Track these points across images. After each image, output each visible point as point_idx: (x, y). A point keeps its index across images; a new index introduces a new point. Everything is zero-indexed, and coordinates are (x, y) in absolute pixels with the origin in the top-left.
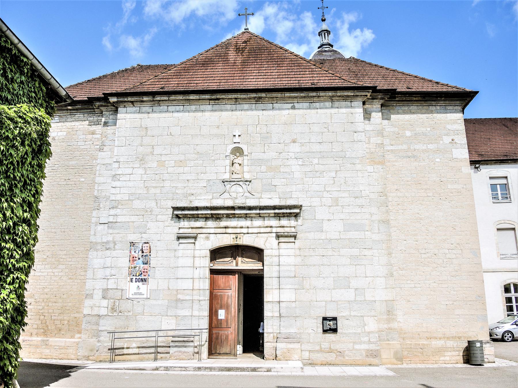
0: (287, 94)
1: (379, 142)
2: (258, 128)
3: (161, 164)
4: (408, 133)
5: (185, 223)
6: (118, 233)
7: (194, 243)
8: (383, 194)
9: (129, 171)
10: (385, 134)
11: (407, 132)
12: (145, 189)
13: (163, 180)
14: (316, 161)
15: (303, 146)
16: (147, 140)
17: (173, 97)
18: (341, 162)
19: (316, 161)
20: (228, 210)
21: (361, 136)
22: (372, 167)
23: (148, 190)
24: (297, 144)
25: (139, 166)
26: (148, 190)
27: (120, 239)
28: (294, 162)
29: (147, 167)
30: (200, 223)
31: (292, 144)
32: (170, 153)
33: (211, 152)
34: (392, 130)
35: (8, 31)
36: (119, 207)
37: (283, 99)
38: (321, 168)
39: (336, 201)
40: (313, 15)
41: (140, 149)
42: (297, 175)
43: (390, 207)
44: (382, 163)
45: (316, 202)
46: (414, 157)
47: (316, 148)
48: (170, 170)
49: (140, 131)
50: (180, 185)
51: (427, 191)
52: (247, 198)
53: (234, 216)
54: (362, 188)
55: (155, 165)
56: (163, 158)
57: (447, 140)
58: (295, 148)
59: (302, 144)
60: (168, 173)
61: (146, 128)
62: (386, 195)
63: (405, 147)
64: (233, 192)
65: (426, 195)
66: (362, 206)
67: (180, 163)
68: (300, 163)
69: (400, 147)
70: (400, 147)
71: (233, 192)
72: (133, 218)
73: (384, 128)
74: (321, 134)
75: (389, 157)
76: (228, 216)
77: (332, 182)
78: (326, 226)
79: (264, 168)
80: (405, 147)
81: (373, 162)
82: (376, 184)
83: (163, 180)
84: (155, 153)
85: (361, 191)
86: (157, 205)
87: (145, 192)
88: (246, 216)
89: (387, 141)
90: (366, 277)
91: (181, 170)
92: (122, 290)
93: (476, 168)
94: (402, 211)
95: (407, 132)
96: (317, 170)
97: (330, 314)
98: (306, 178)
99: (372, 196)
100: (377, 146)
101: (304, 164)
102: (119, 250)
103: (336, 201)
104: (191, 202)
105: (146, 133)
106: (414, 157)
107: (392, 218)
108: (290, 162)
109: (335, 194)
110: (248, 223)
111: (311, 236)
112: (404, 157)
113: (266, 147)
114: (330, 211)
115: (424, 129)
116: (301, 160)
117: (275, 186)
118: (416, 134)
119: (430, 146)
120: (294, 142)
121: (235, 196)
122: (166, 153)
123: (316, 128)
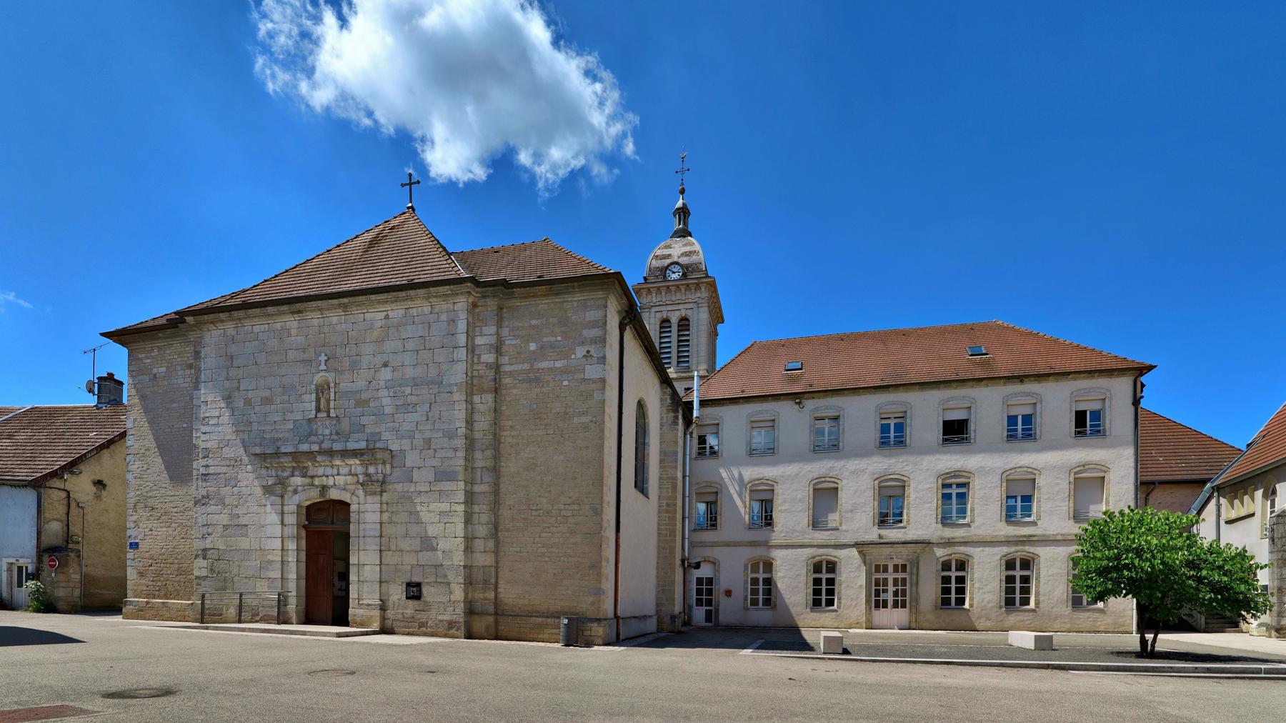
0: (373, 297)
3: (248, 402)
4: (533, 346)
14: (408, 390)
16: (233, 372)
17: (250, 311)
19: (408, 390)
20: (1186, 660)
37: (396, 300)
38: (414, 399)
39: (428, 442)
40: (621, 97)
42: (388, 410)
47: (410, 372)
50: (267, 428)
52: (334, 441)
55: (241, 404)
56: (250, 395)
57: (580, 351)
58: (386, 374)
63: (526, 366)
69: (520, 367)
70: (520, 367)
72: (224, 469)
78: (416, 475)
79: (352, 402)
80: (526, 366)
91: (267, 408)
93: (799, 403)
97: (416, 579)
103: (428, 442)
109: (428, 435)
111: (399, 487)
115: (553, 339)
119: (559, 364)
120: (386, 365)
123: (410, 345)
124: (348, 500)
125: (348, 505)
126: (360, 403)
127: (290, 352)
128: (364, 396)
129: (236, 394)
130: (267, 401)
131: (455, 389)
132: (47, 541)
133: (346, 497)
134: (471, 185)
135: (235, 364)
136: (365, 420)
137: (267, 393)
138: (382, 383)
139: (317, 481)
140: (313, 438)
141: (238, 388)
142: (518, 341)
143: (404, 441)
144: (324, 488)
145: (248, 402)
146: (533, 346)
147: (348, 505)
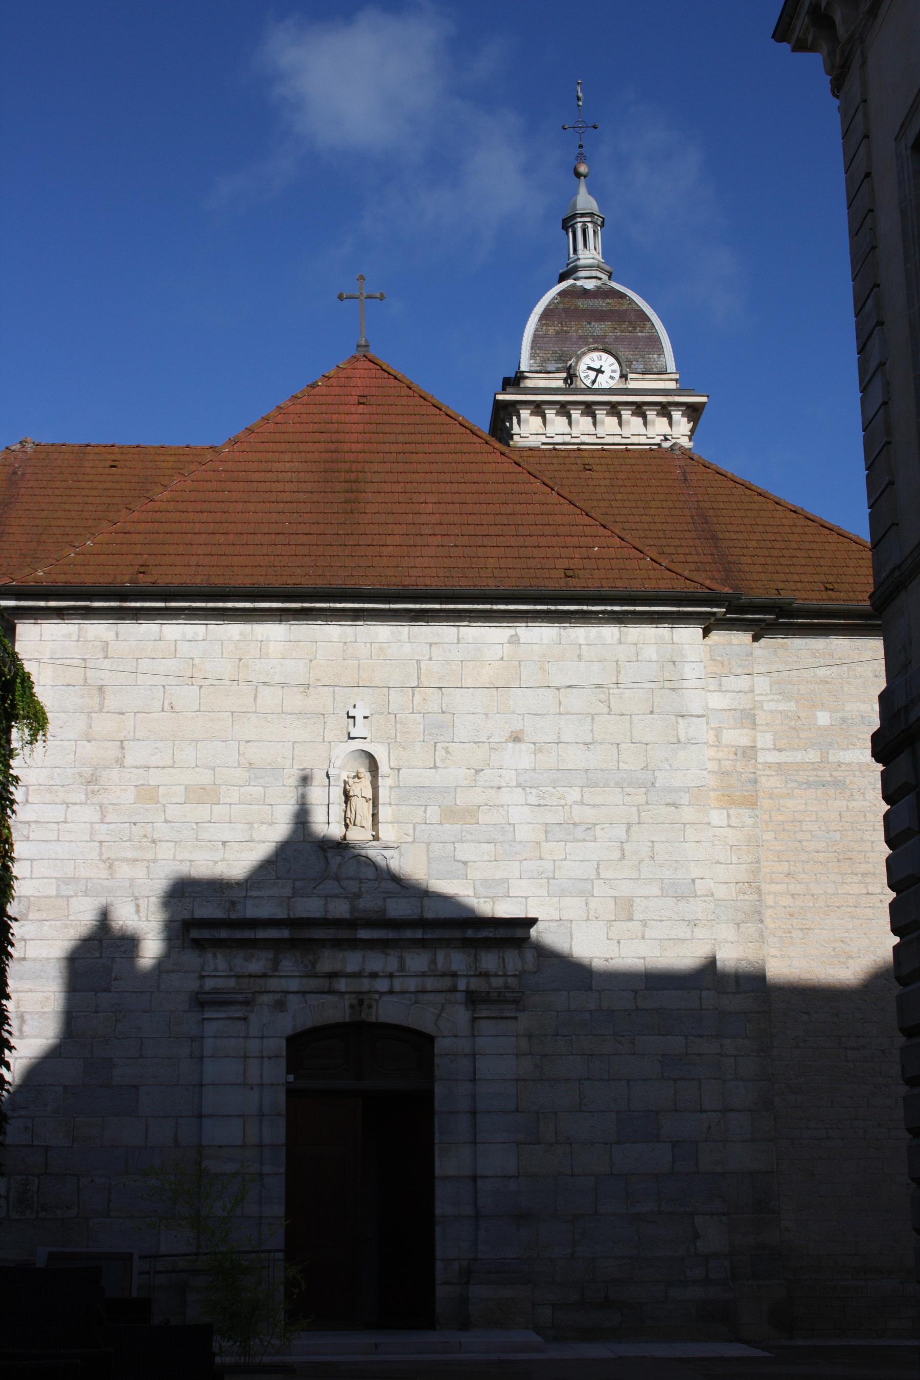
1: (745, 741)
2: (417, 698)
4: (823, 718)
5: (217, 962)
6: (31, 991)
7: (245, 1019)
8: (753, 885)
9: (57, 813)
10: (761, 718)
11: (819, 714)
12: (102, 865)
13: (154, 842)
14: (574, 794)
15: (540, 751)
18: (642, 799)
19: (574, 794)
21: (699, 730)
22: (725, 812)
23: (110, 867)
24: (523, 746)
25: (83, 798)
26: (110, 867)
27: (38, 1008)
28: (518, 796)
29: (106, 801)
30: (257, 965)
31: (511, 745)
32: (170, 763)
33: (288, 762)
34: (782, 707)
35: (223, 1015)
36: (31, 916)
38: (589, 814)
41: (87, 749)
42: (523, 833)
43: (769, 923)
44: (751, 802)
45: (573, 907)
46: (837, 784)
47: (576, 758)
48: (173, 812)
49: (82, 697)
51: (868, 880)
53: (355, 944)
54: (695, 872)
55: (129, 796)
56: (154, 778)
58: (520, 757)
59: (538, 747)
60: (166, 821)
61: (101, 688)
62: (759, 890)
63: (813, 756)
64: (351, 878)
65: (865, 891)
66: (693, 924)
67: (202, 795)
68: (533, 800)
69: (799, 756)
70: (799, 756)
71: (351, 878)
73: (761, 702)
74: (589, 719)
75: (768, 782)
76: (337, 944)
77: (617, 855)
79: (433, 813)
81: (729, 800)
82: (735, 860)
83: (154, 842)
84: (128, 761)
85: (693, 881)
86: (138, 911)
87: (104, 874)
88: (384, 945)
89: (764, 740)
90: (702, 1111)
91: (202, 812)
92: (47, 1148)
94: (800, 934)
95: (819, 714)
96: (577, 820)
98: (547, 841)
99: (721, 892)
100: (740, 753)
101: (542, 802)
102: (35, 1037)
104: (233, 903)
105: (102, 705)
106: (837, 784)
107: (773, 952)
108: (505, 797)
110: (389, 962)
112: (808, 784)
113: (441, 753)
114: (611, 935)
116: (534, 791)
117: (465, 863)
118: (844, 720)
120: (516, 738)
121: (356, 890)
122: (162, 764)
124: (429, 1029)
125: (429, 1039)
126: (451, 814)
127: (264, 692)
128: (463, 799)
129: (115, 773)
130: (202, 795)
131: (685, 798)
132: (659, 893)
133: (421, 1019)
134: (884, 640)
135: (111, 703)
136: (465, 852)
137: (204, 777)
138: (510, 777)
139: (342, 985)
140: (330, 886)
141: (120, 763)
142: (792, 706)
143: (568, 901)
144: (361, 1000)
145: (148, 794)
146: (823, 718)
147: (429, 1039)
